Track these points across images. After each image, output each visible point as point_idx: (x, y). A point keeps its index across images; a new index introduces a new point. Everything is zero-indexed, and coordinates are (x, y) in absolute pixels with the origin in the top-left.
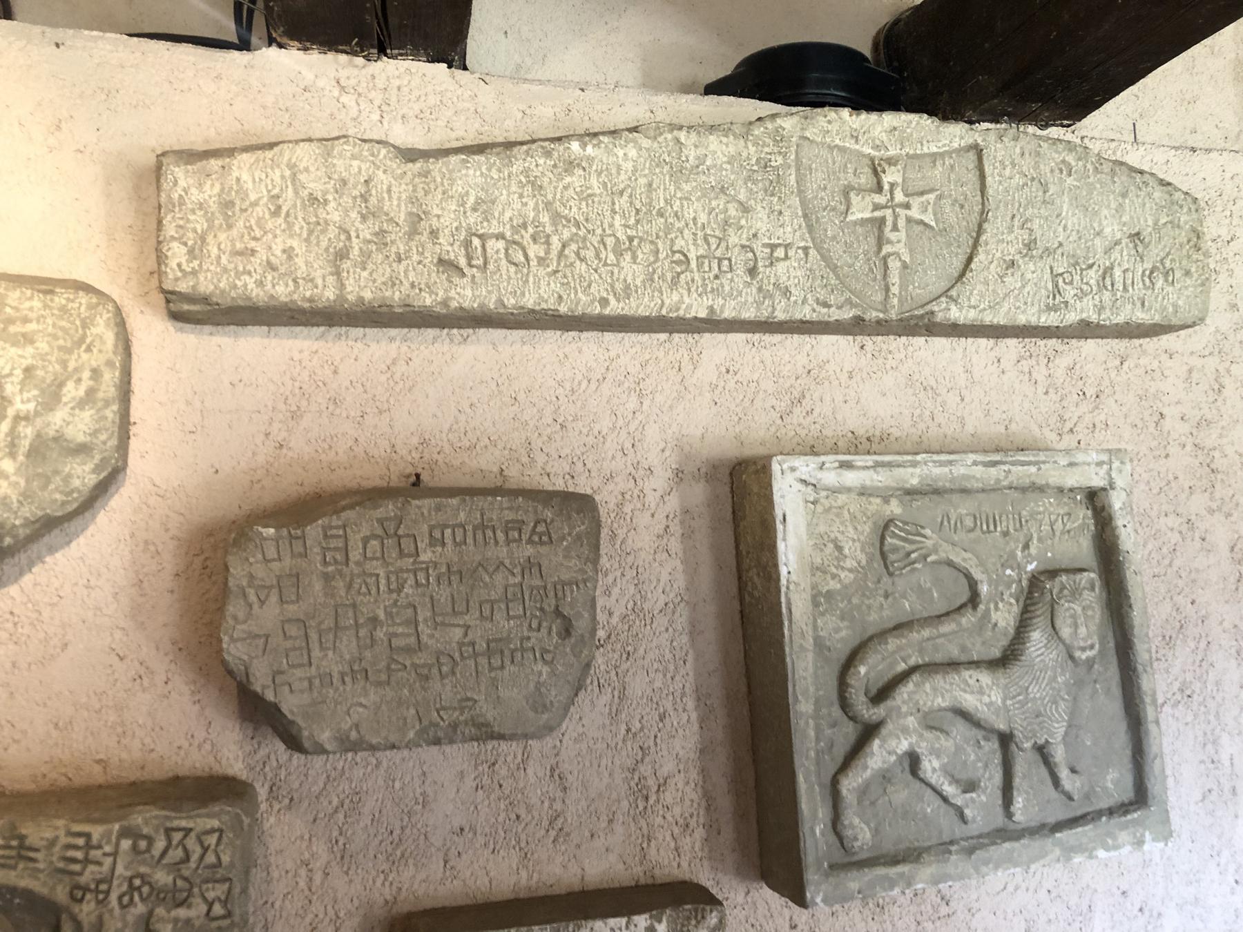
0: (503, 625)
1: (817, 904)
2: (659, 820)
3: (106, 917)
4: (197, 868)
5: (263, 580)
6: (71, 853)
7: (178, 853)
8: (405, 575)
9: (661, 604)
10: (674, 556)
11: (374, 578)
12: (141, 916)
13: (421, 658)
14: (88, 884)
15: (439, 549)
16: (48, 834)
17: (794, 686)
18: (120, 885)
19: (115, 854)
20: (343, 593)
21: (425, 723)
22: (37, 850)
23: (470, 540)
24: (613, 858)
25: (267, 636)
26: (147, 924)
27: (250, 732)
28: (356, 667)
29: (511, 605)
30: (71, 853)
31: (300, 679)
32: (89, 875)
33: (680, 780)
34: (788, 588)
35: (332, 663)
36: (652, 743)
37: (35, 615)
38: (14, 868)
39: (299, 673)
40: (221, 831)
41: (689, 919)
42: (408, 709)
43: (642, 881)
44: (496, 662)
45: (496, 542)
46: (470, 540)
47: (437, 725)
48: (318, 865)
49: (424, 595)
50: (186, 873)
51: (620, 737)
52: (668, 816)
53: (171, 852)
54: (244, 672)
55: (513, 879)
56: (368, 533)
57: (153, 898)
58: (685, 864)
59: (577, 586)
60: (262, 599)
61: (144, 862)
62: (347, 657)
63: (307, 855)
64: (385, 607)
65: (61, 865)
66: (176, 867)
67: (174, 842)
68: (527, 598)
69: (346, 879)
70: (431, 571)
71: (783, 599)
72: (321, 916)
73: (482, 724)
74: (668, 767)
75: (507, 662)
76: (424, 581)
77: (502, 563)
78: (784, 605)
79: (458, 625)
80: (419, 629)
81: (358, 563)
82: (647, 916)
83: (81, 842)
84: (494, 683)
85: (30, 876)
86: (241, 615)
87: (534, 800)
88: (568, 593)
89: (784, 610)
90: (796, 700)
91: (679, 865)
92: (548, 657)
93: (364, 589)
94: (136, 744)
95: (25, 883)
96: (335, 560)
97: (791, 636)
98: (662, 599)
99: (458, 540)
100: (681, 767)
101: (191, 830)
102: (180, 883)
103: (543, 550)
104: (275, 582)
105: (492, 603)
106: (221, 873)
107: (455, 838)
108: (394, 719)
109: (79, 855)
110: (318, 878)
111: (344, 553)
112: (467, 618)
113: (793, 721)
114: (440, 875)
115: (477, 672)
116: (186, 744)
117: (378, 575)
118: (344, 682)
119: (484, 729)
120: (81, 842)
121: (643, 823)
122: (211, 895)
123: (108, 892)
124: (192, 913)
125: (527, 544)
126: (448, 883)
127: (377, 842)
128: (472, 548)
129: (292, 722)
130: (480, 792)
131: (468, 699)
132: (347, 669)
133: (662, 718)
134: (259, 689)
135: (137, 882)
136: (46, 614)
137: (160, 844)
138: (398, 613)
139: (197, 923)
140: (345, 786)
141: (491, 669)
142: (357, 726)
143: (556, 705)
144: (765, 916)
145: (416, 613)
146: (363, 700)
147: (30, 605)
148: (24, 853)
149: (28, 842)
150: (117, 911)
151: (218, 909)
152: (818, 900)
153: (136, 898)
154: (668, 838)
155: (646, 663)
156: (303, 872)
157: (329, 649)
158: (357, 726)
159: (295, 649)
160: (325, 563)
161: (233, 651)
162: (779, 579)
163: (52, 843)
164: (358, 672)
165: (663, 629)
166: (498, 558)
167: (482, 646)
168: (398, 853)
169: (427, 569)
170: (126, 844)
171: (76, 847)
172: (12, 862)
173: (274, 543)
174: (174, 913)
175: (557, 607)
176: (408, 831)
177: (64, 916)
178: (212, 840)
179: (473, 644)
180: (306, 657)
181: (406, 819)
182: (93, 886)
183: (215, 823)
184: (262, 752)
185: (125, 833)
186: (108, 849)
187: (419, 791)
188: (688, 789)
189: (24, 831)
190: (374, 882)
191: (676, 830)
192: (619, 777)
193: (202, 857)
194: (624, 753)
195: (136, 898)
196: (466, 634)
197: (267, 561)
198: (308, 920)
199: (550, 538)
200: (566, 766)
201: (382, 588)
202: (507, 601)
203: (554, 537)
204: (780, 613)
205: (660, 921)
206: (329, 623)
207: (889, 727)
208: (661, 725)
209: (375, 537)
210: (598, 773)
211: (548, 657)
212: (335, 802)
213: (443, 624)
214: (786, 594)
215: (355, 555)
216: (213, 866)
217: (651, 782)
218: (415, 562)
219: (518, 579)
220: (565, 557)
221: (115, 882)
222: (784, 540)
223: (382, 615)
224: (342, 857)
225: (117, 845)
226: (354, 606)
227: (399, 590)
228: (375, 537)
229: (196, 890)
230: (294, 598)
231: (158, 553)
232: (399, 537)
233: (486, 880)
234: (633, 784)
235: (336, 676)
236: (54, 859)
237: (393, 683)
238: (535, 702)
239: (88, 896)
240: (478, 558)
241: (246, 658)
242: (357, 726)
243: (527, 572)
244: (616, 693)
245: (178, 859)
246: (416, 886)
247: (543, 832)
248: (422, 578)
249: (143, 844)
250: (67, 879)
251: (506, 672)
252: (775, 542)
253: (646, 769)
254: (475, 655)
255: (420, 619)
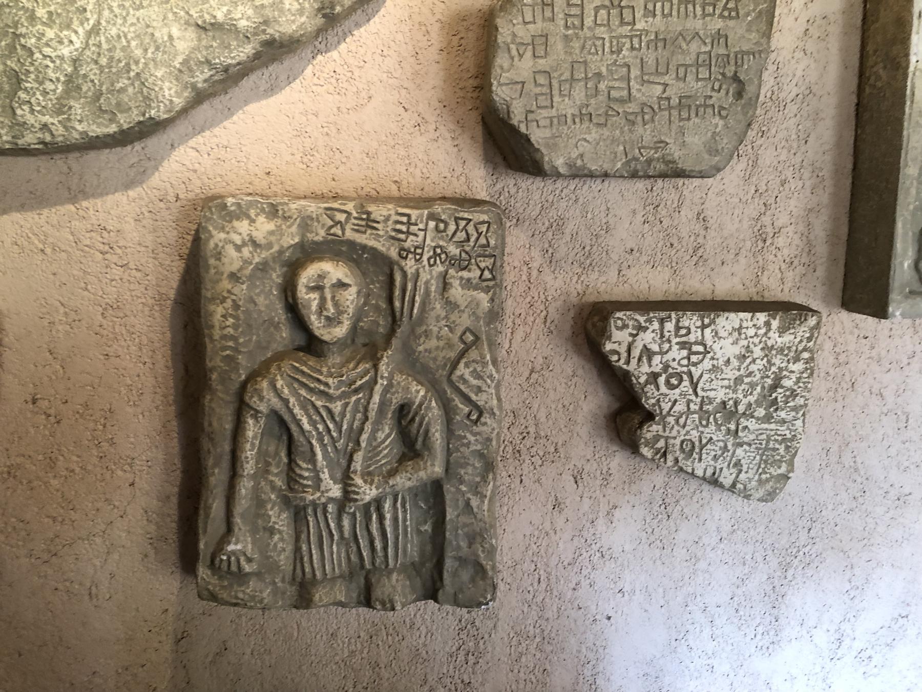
0: (693, 85)
1: (895, 316)
2: (771, 257)
3: (421, 270)
4: (474, 246)
5: (522, 38)
6: (399, 227)
7: (461, 236)
8: (624, 40)
9: (793, 94)
10: (809, 55)
11: (601, 42)
12: (441, 273)
13: (632, 107)
14: (409, 248)
15: (650, 19)
16: (385, 213)
17: (906, 154)
18: (428, 252)
19: (425, 230)
20: (577, 51)
21: (630, 157)
22: (378, 222)
23: (674, 13)
24: (736, 280)
25: (523, 83)
26: (445, 277)
27: (491, 171)
28: (584, 112)
29: (700, 69)
30: (399, 227)
31: (545, 118)
32: (410, 242)
33: (791, 229)
34: (914, 74)
35: (567, 107)
36: (773, 202)
37: (349, 74)
38: (365, 232)
39: (545, 113)
40: (489, 223)
41: (795, 320)
42: (618, 146)
43: (755, 298)
44: (685, 114)
45: (695, 16)
46: (674, 13)
47: (637, 159)
48: (535, 265)
49: (637, 57)
50: (467, 249)
51: (750, 195)
52: (779, 254)
53: (458, 233)
54: (506, 111)
55: (665, 287)
56: (599, 4)
57: (447, 263)
58: (786, 290)
59: (754, 56)
60: (521, 52)
61: (442, 238)
62: (578, 103)
63: (528, 259)
64: (608, 65)
65: (393, 234)
66: (460, 244)
67: (461, 228)
68: (713, 63)
69: (553, 276)
70: (643, 37)
71: (909, 84)
72: (536, 298)
73: (670, 162)
74: (782, 220)
75: (693, 115)
76: (637, 46)
77: (697, 33)
78: (909, 88)
79: (659, 83)
80: (631, 84)
81: (589, 28)
82: (766, 314)
83: (405, 219)
84: (682, 132)
85: (375, 239)
86: (506, 65)
87: (684, 234)
88: (746, 62)
89: (908, 92)
90: (906, 165)
91: (782, 291)
92: (724, 113)
93: (593, 50)
94: (418, 173)
95: (372, 243)
96: (574, 24)
97: (910, 114)
98: (795, 91)
99: (666, 12)
100: (793, 220)
101: (470, 220)
102: (463, 255)
103: (731, 23)
104: (530, 41)
105: (686, 66)
106: (489, 251)
107: (627, 256)
108: (608, 153)
109: (404, 228)
110: (535, 273)
111: (580, 20)
112: (667, 77)
113: (901, 181)
114: (615, 280)
115: (670, 122)
116: (449, 175)
117: (604, 39)
118: (574, 123)
119: (671, 166)
120: (405, 219)
121: (760, 258)
122: (483, 265)
123: (422, 254)
124: (471, 275)
125: (718, 18)
126: (621, 287)
127: (573, 253)
128: (675, 19)
129: (538, 150)
130: (646, 225)
131: (662, 142)
132: (577, 113)
133: (783, 183)
134: (516, 124)
135: (438, 251)
136: (357, 73)
137: (452, 227)
138: (616, 70)
139: (474, 282)
140: (553, 213)
141: (681, 120)
142: (582, 156)
143: (726, 151)
144: (840, 333)
145: (629, 71)
146: (588, 137)
147: (346, 67)
148: (370, 224)
149: (373, 216)
150: (427, 267)
151: (487, 275)
152: (898, 313)
153: (438, 262)
154: (777, 271)
155: (776, 139)
156: (525, 268)
157: (565, 95)
158: (581, 156)
159: (543, 94)
160: (567, 27)
161: (499, 92)
162: (907, 67)
163: (387, 219)
164: (585, 116)
165: (792, 115)
166: (695, 29)
167: (675, 101)
168: (588, 262)
169: (640, 36)
170: (432, 224)
171: (402, 223)
172: (363, 229)
173: (531, 8)
174: (460, 274)
175: (736, 72)
176: (595, 248)
177: (396, 267)
178: (483, 228)
179: (669, 99)
180: (549, 101)
181: (594, 240)
182: (412, 250)
183: (485, 217)
184: (499, 186)
185: (431, 217)
186: (421, 226)
187: (604, 221)
188: (796, 237)
189: (370, 209)
190: (571, 280)
191: (784, 266)
192: (746, 224)
193: (478, 239)
194: (752, 207)
195: (438, 262)
196: (664, 91)
197: (526, 23)
198: (528, 300)
199: (738, 13)
200: (709, 212)
201: (606, 50)
202: (698, 65)
203: (741, 12)
204: (904, 95)
205: (775, 319)
206: (567, 75)
207: (634, 461)
208: (781, 189)
209: (604, 7)
210: (732, 220)
211: (724, 113)
212: (547, 224)
213: (649, 82)
214: (913, 79)
215: (589, 21)
216: (483, 246)
217: (769, 230)
218: (631, 30)
219: (708, 48)
220: (747, 31)
221: (426, 249)
222: (918, 33)
223: (604, 70)
224: (551, 262)
225: (427, 224)
226: (585, 62)
227: (619, 51)
228: (604, 7)
229: (473, 261)
230: (543, 53)
231: (428, 32)
232: (622, 8)
233: (647, 286)
234: (756, 230)
235: (569, 116)
236: (389, 229)
237: (609, 125)
238: (710, 147)
239: (410, 256)
240: (679, 28)
241: (508, 99)
242: (582, 156)
243: (716, 42)
244: (751, 163)
245: (462, 239)
246: (599, 285)
247: (689, 257)
248: (636, 41)
249: (442, 226)
250: (397, 243)
251: (691, 122)
252: (910, 35)
253: (766, 220)
254: (670, 108)
255: (632, 76)
